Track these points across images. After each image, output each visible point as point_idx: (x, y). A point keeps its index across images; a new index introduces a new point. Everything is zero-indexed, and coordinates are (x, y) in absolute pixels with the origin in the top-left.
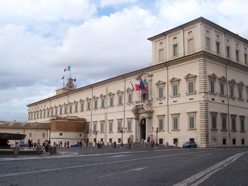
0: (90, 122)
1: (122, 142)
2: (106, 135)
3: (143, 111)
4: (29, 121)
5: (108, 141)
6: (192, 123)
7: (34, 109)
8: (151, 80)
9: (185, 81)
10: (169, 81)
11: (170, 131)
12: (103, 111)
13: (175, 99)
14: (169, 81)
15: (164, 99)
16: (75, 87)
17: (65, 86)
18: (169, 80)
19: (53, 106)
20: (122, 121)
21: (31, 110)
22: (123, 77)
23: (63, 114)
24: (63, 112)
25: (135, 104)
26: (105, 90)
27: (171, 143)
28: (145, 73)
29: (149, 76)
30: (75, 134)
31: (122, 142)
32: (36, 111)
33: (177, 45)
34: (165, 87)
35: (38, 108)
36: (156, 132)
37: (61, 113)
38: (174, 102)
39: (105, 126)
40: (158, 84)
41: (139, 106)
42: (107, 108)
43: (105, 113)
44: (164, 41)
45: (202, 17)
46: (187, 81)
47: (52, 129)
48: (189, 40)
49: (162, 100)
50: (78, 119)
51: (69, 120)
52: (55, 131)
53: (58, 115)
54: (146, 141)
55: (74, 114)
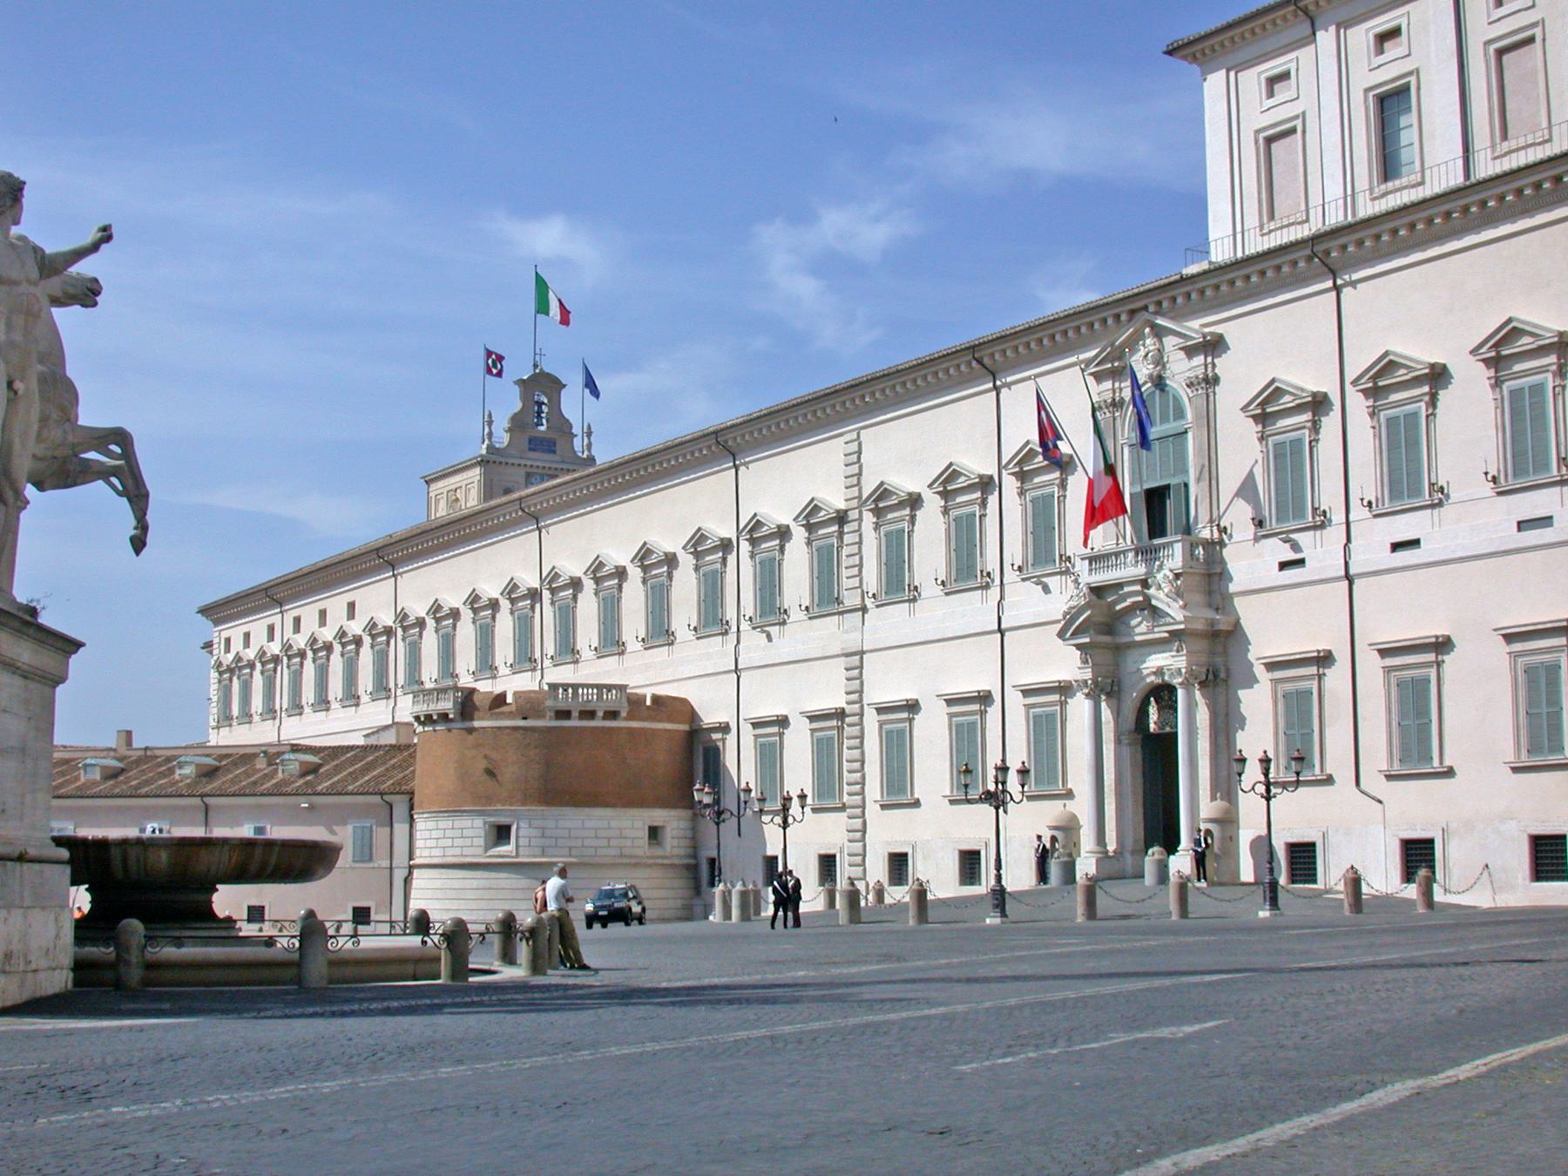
0: (725, 728)
1: (999, 878)
2: (857, 823)
3: (1150, 631)
4: (224, 731)
5: (878, 870)
6: (1545, 710)
7: (310, 624)
8: (1206, 380)
9: (1483, 374)
10: (1354, 383)
11: (1373, 780)
12: (831, 633)
13: (1404, 527)
14: (1349, 378)
15: (1432, 506)
16: (577, 443)
17: (502, 439)
18: (1350, 375)
19: (419, 609)
20: (983, 713)
21: (237, 645)
22: (980, 362)
23: (503, 671)
24: (504, 651)
25: (1089, 577)
26: (842, 471)
27: (1384, 878)
28: (1153, 326)
29: (1190, 351)
30: (442, 824)
31: (999, 878)
32: (275, 648)
33: (1406, 89)
34: (727, 569)
35: (297, 629)
36: (1261, 789)
37: (486, 665)
38: (1396, 547)
39: (846, 754)
40: (1265, 410)
41: (1120, 586)
42: (864, 609)
43: (847, 655)
44: (1299, 60)
45: (571, 316)
46: (1497, 383)
47: (423, 785)
48: (1501, 53)
49: (1303, 538)
50: (636, 702)
51: (564, 714)
52: (452, 809)
53: (466, 681)
54: (1181, 863)
55: (593, 670)
